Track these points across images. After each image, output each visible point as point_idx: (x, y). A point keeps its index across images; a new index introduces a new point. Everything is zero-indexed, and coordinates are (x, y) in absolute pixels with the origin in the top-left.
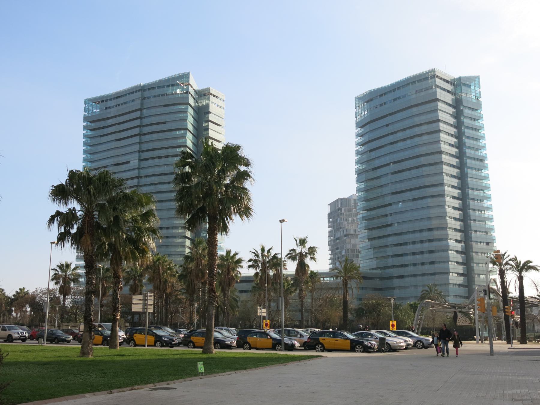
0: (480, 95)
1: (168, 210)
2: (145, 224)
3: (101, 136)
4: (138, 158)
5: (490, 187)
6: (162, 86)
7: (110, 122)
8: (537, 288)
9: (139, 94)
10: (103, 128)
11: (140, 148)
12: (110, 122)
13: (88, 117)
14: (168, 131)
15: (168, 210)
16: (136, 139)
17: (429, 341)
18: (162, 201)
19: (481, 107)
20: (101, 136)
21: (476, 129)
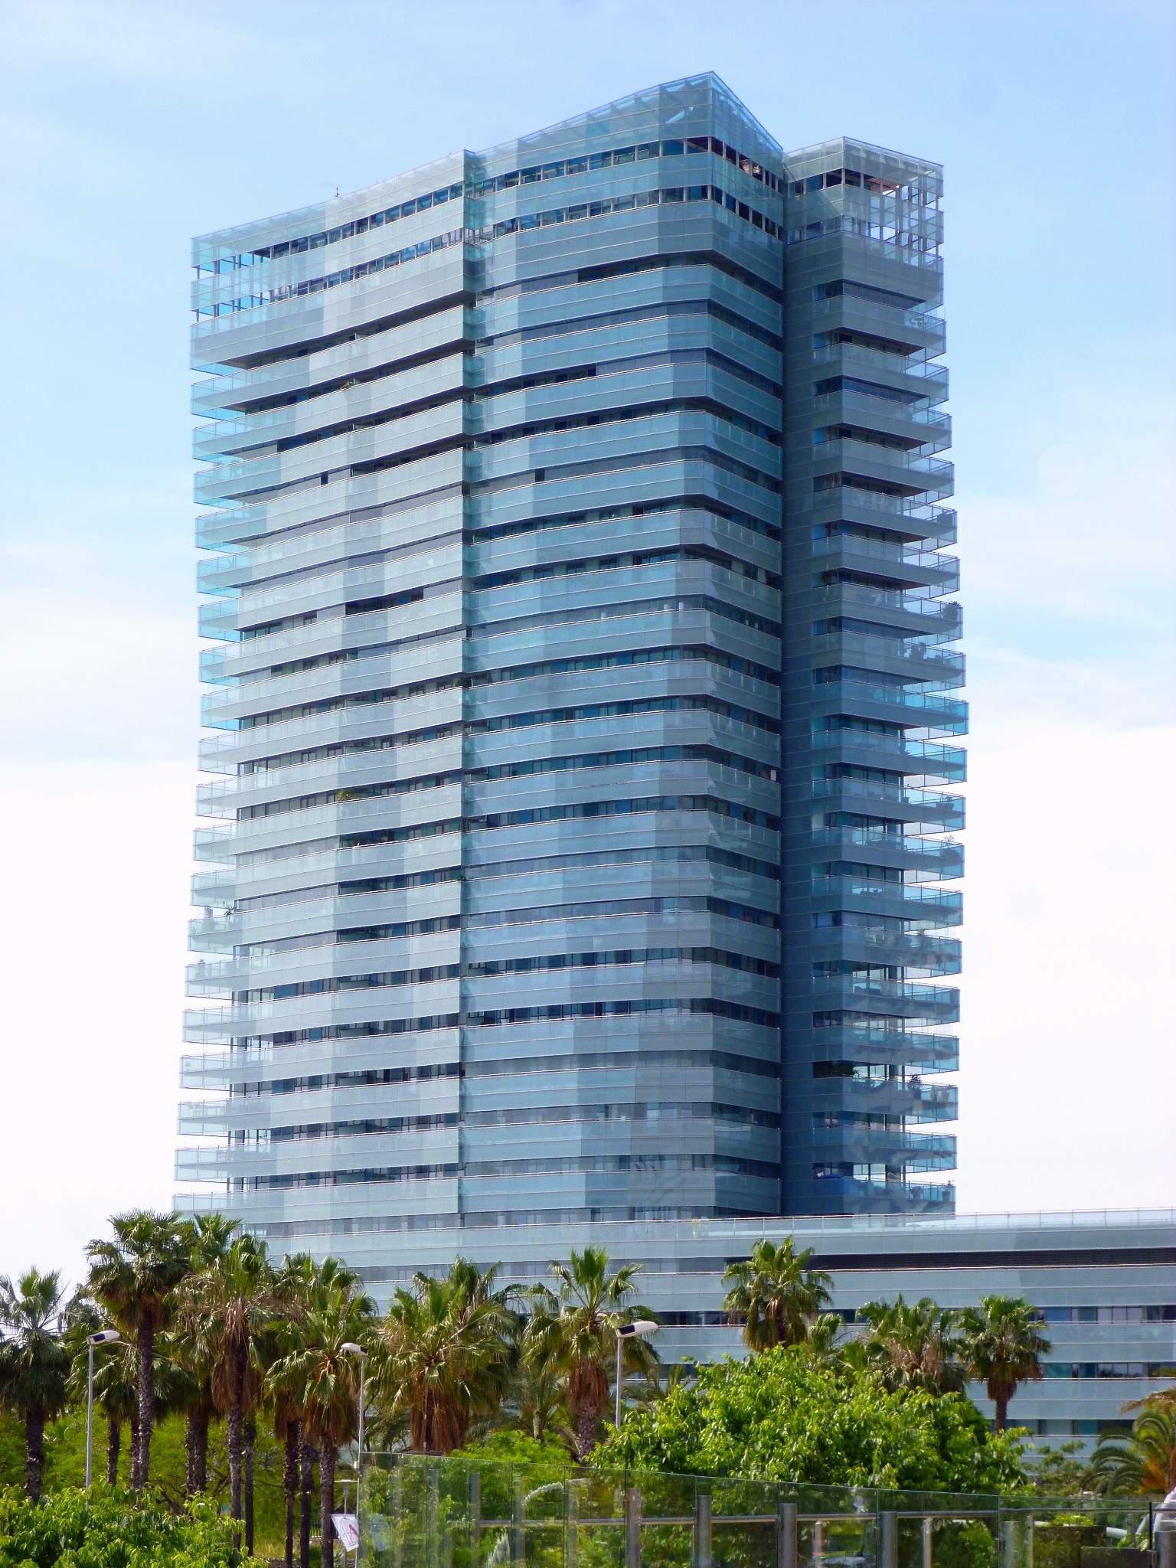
0: (940, 227)
1: (625, 855)
2: (879, 939)
3: (284, 445)
4: (458, 571)
5: (963, 671)
6: (570, 162)
7: (321, 366)
8: (422, 1171)
9: (450, 215)
10: (291, 398)
11: (469, 517)
12: (321, 366)
13: (217, 337)
14: (394, 418)
15: (625, 855)
16: (450, 467)
17: (1077, 1467)
18: (591, 809)
19: (939, 289)
20: (284, 445)
21: (907, 395)
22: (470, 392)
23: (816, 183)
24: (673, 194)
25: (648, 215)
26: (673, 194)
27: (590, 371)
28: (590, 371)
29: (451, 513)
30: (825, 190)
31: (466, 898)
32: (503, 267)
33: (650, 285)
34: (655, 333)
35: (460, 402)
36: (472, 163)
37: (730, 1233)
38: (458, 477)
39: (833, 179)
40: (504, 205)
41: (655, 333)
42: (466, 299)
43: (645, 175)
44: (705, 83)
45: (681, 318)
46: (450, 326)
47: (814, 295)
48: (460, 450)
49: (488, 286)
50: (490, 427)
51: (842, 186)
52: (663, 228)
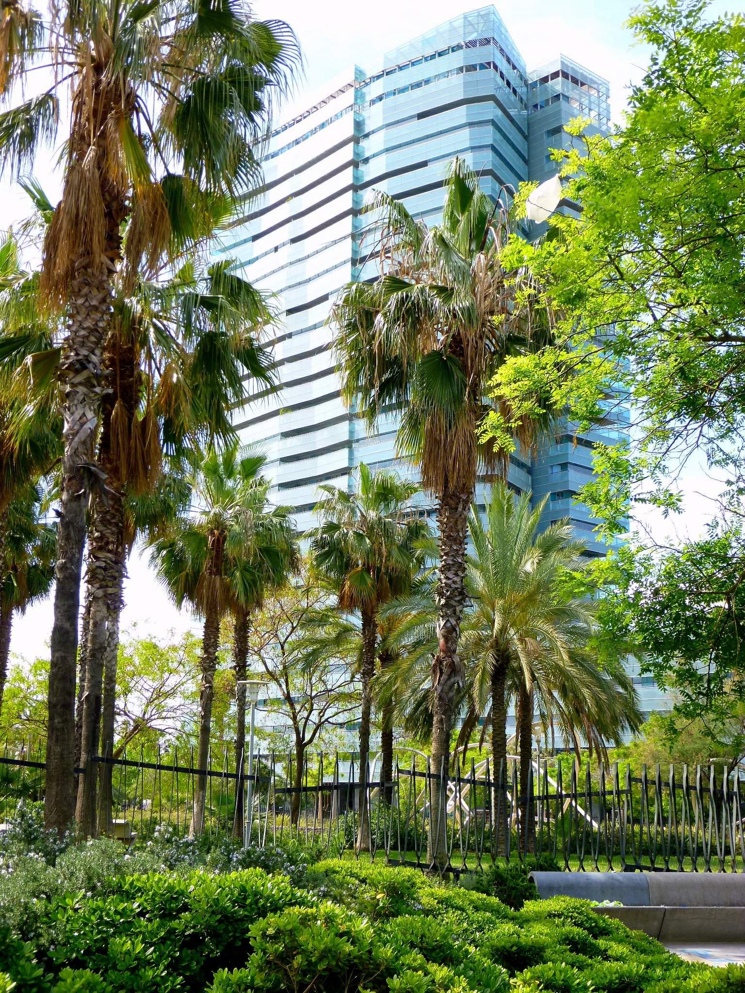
3: (255, 238)
20: (255, 238)
22: (357, 187)
23: (545, 80)
24: (471, 68)
25: (458, 80)
26: (471, 68)
27: (424, 164)
28: (424, 164)
29: (345, 250)
30: (550, 82)
31: (351, 458)
32: (374, 117)
33: (460, 115)
34: (463, 138)
35: (351, 216)
36: (359, 73)
37: (77, 820)
38: (349, 255)
39: (555, 75)
40: (375, 89)
41: (463, 138)
42: (356, 140)
43: (457, 59)
44: (488, 14)
45: (476, 129)
46: (347, 154)
47: (545, 136)
48: (347, 422)
49: (366, 132)
50: (367, 179)
51: (560, 78)
52: (466, 84)
